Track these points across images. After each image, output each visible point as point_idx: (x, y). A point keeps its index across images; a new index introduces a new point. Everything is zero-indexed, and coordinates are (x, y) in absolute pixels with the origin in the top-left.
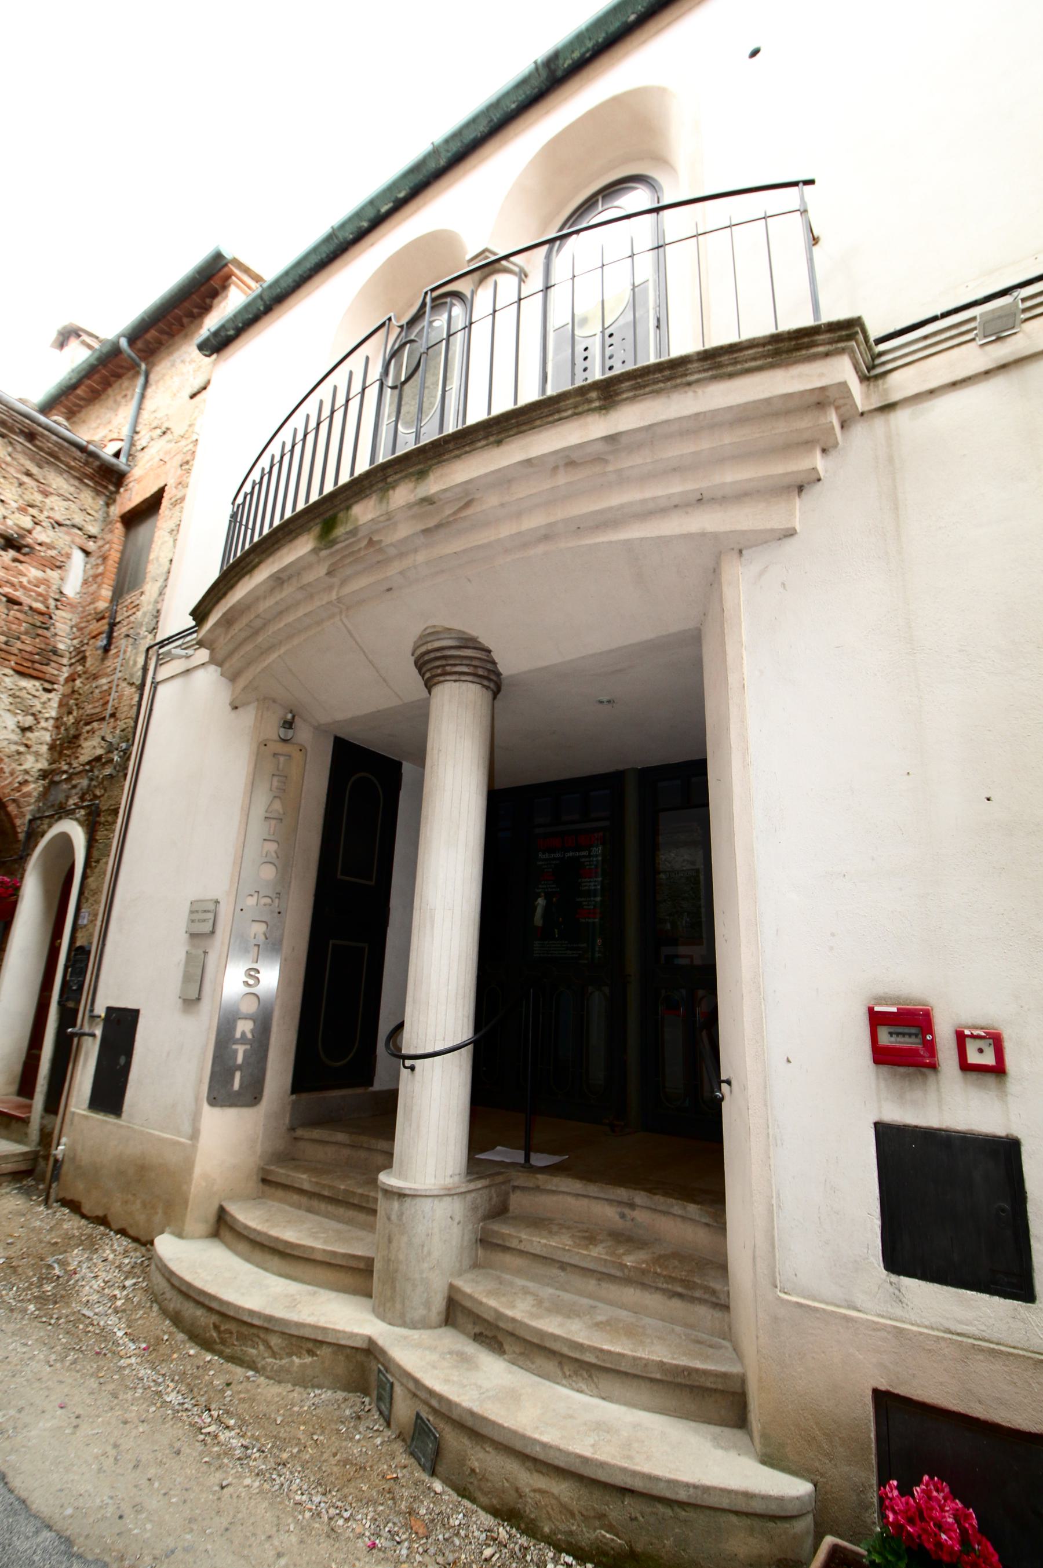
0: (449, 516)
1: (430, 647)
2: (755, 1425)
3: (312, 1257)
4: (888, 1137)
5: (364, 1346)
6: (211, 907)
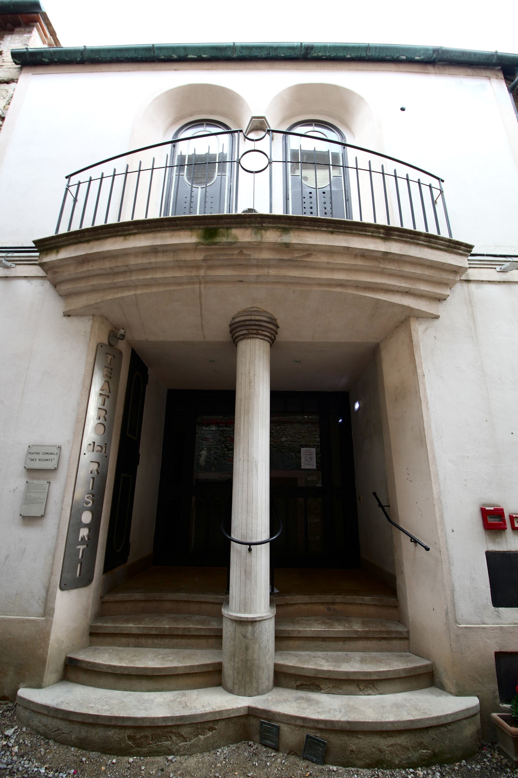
0: (297, 257)
1: (253, 318)
2: (446, 681)
3: (176, 673)
4: (490, 556)
5: (246, 713)
6: (55, 450)
